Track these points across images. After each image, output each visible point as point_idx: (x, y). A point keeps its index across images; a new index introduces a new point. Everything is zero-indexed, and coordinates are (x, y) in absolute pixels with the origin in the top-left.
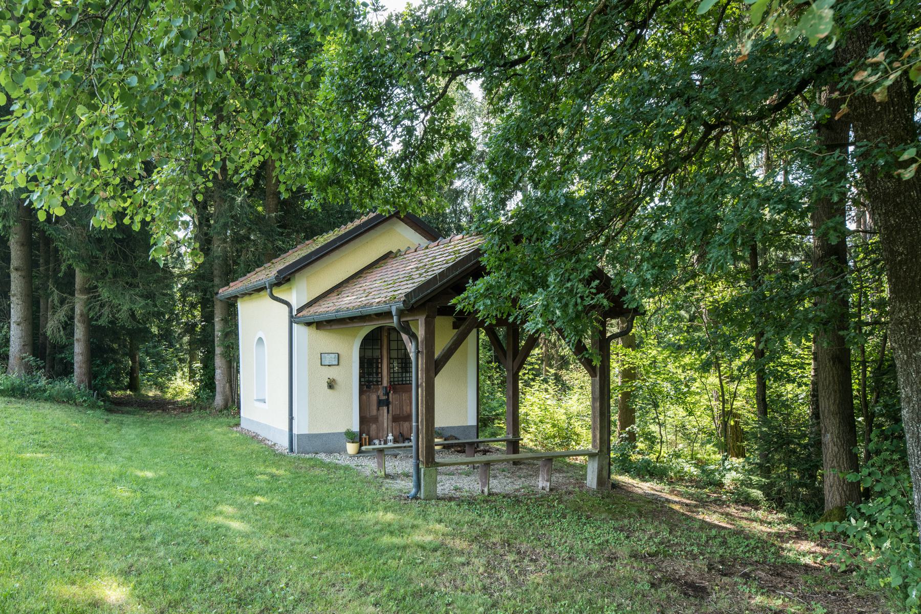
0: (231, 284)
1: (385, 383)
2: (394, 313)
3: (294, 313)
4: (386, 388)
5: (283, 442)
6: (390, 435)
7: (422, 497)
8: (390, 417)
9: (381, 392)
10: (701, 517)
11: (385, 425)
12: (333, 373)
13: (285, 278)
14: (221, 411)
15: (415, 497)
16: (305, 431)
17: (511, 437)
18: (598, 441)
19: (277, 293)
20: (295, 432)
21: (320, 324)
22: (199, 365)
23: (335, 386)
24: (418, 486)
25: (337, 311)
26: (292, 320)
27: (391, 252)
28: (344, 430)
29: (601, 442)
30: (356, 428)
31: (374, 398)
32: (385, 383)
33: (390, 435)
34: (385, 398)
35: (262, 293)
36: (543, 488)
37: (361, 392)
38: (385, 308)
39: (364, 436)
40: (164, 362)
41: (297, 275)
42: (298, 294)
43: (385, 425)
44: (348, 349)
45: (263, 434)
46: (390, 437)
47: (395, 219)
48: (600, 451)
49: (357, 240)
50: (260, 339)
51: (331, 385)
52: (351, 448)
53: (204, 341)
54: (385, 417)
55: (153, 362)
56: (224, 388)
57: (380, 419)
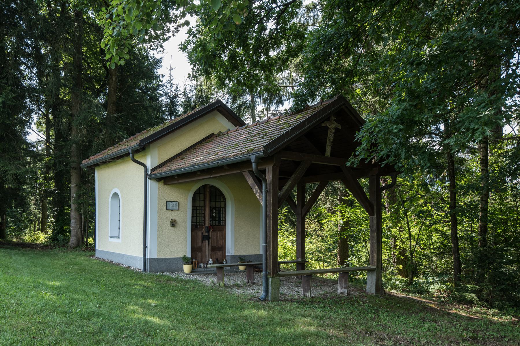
0: (91, 157)
1: (207, 224)
2: (253, 161)
3: (149, 172)
4: (208, 227)
5: (139, 266)
6: (211, 260)
7: (270, 300)
8: (210, 248)
9: (204, 231)
10: (454, 311)
11: (207, 253)
12: (174, 215)
13: (143, 148)
14: (75, 248)
15: (265, 299)
16: (155, 257)
17: (300, 260)
18: (376, 260)
19: (137, 157)
20: (148, 256)
21: (167, 180)
22: (52, 219)
23: (176, 225)
24: (267, 291)
25: (193, 166)
26: (147, 177)
27: (213, 134)
28: (182, 256)
29: (377, 261)
30: (189, 255)
31: (200, 234)
32: (207, 224)
33: (211, 260)
34: (207, 234)
35: (126, 158)
36: (342, 293)
37: (193, 230)
38: (244, 158)
39: (195, 260)
40: (20, 221)
41: (151, 145)
42: (150, 161)
43: (207, 253)
44: (184, 198)
45: (116, 261)
46: (211, 261)
47: (216, 111)
48: (377, 267)
49: (192, 124)
50: (116, 195)
51: (173, 224)
52: (187, 268)
53: (61, 201)
54: (207, 247)
55: (12, 221)
56: (77, 232)
57: (203, 249)
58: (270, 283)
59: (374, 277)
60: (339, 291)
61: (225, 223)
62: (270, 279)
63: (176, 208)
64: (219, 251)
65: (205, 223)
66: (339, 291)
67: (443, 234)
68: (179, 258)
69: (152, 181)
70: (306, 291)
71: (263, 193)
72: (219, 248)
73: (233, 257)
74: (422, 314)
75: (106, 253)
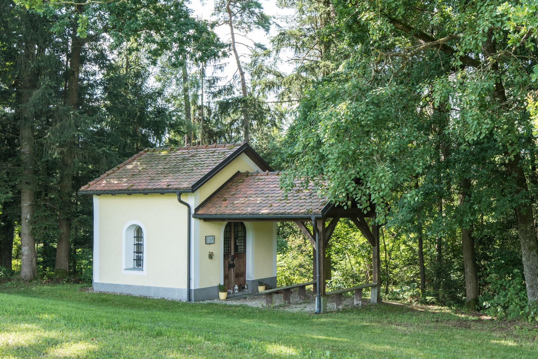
1: (232, 254)
3: (193, 212)
5: (184, 297)
6: (236, 286)
16: (198, 287)
20: (192, 287)
32: (232, 254)
36: (357, 304)
43: (232, 280)
44: (218, 232)
51: (211, 256)
52: (223, 295)
57: (230, 276)
58: (322, 301)
59: (376, 291)
60: (355, 303)
61: (246, 251)
62: (322, 299)
63: (213, 242)
64: (241, 276)
65: (230, 252)
66: (355, 303)
67: (411, 249)
68: (215, 287)
69: (196, 219)
70: (338, 305)
71: (317, 240)
72: (241, 274)
73: (254, 281)
74: (409, 313)
75: (103, 284)
